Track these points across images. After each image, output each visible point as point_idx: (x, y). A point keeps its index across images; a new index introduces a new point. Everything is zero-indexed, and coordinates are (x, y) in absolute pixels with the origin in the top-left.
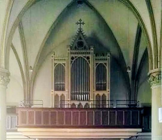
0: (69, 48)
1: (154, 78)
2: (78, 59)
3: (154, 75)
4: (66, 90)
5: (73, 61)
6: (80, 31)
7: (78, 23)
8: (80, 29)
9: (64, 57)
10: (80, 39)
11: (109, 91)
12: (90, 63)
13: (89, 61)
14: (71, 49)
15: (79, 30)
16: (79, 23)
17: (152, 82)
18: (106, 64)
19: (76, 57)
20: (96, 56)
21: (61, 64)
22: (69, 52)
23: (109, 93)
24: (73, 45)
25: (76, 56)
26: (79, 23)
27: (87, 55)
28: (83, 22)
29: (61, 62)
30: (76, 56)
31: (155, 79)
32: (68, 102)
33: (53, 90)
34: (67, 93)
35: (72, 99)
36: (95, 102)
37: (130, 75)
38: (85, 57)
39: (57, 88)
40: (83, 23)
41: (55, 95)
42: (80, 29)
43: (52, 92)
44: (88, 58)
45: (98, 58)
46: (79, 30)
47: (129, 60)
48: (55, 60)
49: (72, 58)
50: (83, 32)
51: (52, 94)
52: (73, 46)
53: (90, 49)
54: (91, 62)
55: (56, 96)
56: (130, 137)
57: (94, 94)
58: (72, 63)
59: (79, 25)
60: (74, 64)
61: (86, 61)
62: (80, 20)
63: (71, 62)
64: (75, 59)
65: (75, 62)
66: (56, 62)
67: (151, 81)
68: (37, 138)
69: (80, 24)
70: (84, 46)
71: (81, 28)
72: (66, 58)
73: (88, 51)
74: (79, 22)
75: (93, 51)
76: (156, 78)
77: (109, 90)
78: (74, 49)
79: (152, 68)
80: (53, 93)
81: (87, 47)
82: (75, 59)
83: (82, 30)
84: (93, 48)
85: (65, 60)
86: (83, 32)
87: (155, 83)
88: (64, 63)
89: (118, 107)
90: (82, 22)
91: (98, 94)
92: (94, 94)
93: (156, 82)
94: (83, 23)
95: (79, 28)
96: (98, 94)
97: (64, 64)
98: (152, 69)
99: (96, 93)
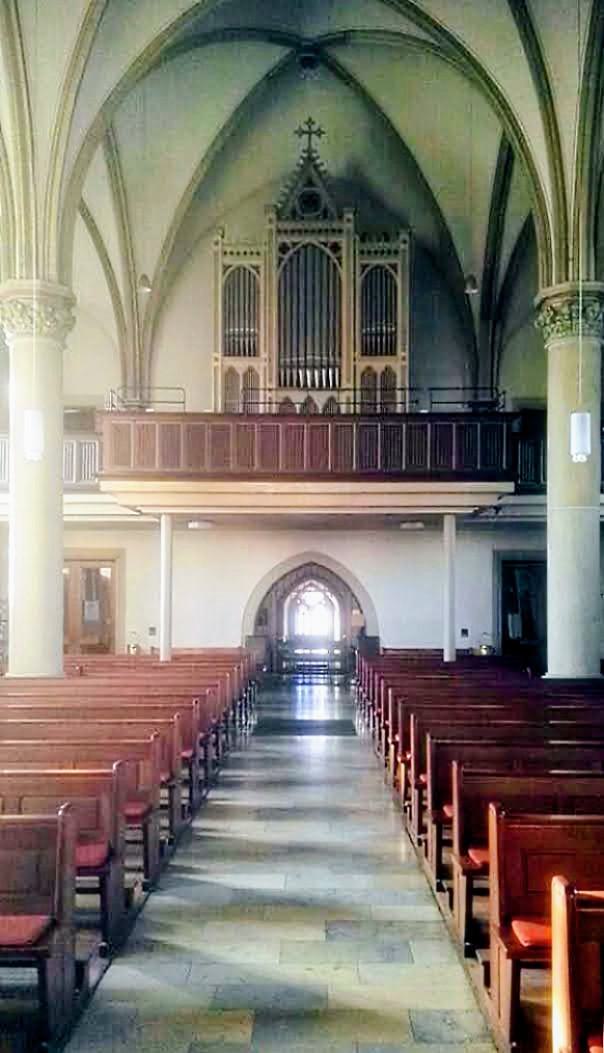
0: (273, 216)
1: (556, 313)
2: (302, 251)
3: (556, 303)
4: (263, 355)
6: (310, 159)
7: (301, 133)
8: (309, 151)
9: (255, 245)
10: (310, 183)
12: (340, 264)
14: (279, 218)
15: (305, 155)
16: (304, 132)
17: (548, 329)
18: (394, 267)
19: (294, 244)
20: (363, 240)
21: (245, 269)
22: (273, 227)
23: (406, 363)
24: (285, 204)
25: (295, 239)
26: (304, 132)
27: (333, 239)
28: (319, 130)
29: (246, 262)
30: (295, 239)
31: (558, 318)
32: (268, 394)
33: (219, 355)
35: (283, 384)
36: (358, 393)
37: (476, 306)
38: (325, 244)
39: (231, 350)
41: (226, 369)
42: (309, 151)
43: (216, 359)
44: (336, 248)
45: (367, 246)
46: (305, 155)
47: (471, 253)
48: (225, 253)
49: (283, 248)
50: (318, 161)
51: (216, 369)
52: (284, 207)
53: (341, 217)
54: (344, 260)
55: (230, 374)
58: (283, 263)
59: (305, 137)
60: (288, 268)
61: (329, 258)
62: (310, 122)
63: (280, 260)
64: (291, 252)
66: (228, 260)
67: (545, 325)
68: (165, 514)
69: (310, 133)
70: (323, 207)
71: (313, 147)
72: (263, 249)
73: (335, 225)
74: (306, 128)
76: (563, 315)
77: (406, 354)
78: (287, 219)
79: (548, 280)
80: (219, 364)
81: (332, 209)
82: (291, 252)
83: (314, 155)
84: (351, 216)
85: (258, 254)
86: (318, 161)
87: (558, 331)
88: (254, 263)
89: (434, 411)
90: (314, 128)
93: (561, 329)
94: (319, 133)
95: (306, 148)
96: (369, 368)
97: (256, 268)
98: (548, 285)
99: (362, 364)
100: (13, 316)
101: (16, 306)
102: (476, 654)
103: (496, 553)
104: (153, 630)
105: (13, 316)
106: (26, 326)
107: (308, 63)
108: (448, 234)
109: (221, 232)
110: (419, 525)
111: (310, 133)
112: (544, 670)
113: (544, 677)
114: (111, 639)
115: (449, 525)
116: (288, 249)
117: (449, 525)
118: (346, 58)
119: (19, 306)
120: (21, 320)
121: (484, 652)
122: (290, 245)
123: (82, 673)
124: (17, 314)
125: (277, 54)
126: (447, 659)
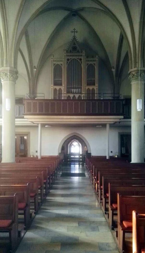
0: (65, 52)
3: (134, 73)
4: (63, 85)
5: (69, 62)
6: (74, 38)
7: (72, 32)
8: (74, 36)
10: (74, 44)
11: (97, 86)
12: (82, 63)
13: (81, 62)
15: (73, 37)
16: (73, 32)
17: (132, 79)
19: (71, 59)
20: (87, 58)
21: (59, 65)
23: (98, 87)
25: (71, 57)
26: (73, 32)
27: (80, 57)
31: (134, 76)
33: (53, 85)
34: (64, 88)
35: (68, 92)
38: (78, 59)
39: (55, 84)
40: (77, 32)
42: (74, 36)
43: (52, 86)
44: (81, 59)
46: (73, 37)
47: (113, 60)
48: (54, 61)
51: (52, 89)
53: (82, 52)
54: (83, 62)
55: (55, 90)
56: (115, 122)
57: (85, 88)
61: (79, 62)
62: (74, 29)
63: (67, 62)
65: (70, 62)
66: (55, 63)
69: (74, 32)
70: (77, 50)
71: (75, 35)
73: (80, 54)
74: (73, 31)
75: (84, 54)
76: (135, 76)
80: (52, 87)
81: (80, 51)
85: (62, 61)
87: (134, 80)
88: (61, 63)
90: (75, 31)
91: (89, 89)
92: (85, 88)
93: (135, 79)
94: (77, 32)
95: (73, 35)
96: (89, 89)
97: (62, 64)
99: (87, 88)
100: (3, 76)
101: (4, 74)
102: (114, 157)
103: (119, 133)
104: (37, 152)
105: (3, 76)
106: (6, 79)
107: (74, 15)
108: (108, 56)
109: (53, 56)
110: (101, 126)
111: (74, 32)
112: (131, 161)
113: (130, 163)
114: (27, 154)
115: (108, 126)
116: (69, 60)
117: (108, 126)
118: (83, 14)
119: (5, 74)
120: (5, 77)
121: (116, 157)
122: (70, 59)
123: (20, 162)
124: (4, 75)
125: (66, 13)
126: (107, 158)
